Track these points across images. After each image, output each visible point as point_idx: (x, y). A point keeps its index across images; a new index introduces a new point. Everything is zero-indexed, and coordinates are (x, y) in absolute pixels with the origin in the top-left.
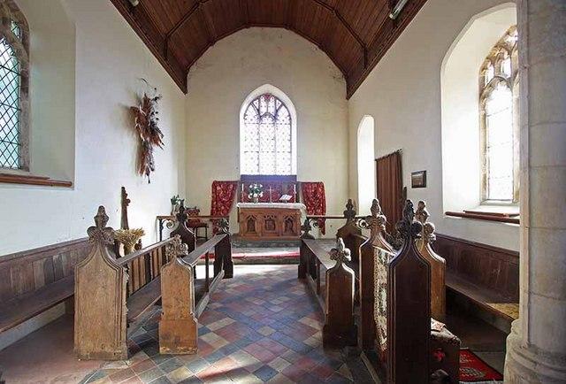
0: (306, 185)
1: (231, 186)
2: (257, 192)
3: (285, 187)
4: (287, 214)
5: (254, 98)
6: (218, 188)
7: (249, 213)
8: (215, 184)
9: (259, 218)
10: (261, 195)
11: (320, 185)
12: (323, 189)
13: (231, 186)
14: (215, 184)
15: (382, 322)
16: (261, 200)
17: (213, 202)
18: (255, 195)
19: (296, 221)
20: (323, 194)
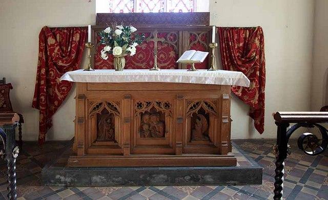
0: (226, 34)
1: (77, 38)
2: (121, 43)
3: (185, 38)
4: (196, 97)
5: (167, 128)
6: (51, 41)
7: (98, 98)
8: (46, 33)
9: (126, 108)
10: (133, 51)
11: (256, 33)
12: (262, 42)
13: (77, 38)
14: (46, 33)
15: (186, 134)
16: (132, 63)
17: (39, 69)
18: (118, 51)
19: (219, 116)
20: (261, 52)
